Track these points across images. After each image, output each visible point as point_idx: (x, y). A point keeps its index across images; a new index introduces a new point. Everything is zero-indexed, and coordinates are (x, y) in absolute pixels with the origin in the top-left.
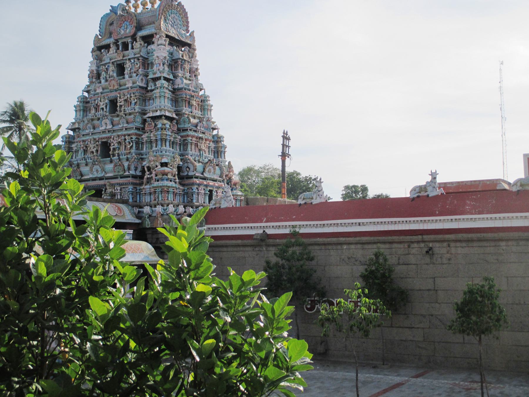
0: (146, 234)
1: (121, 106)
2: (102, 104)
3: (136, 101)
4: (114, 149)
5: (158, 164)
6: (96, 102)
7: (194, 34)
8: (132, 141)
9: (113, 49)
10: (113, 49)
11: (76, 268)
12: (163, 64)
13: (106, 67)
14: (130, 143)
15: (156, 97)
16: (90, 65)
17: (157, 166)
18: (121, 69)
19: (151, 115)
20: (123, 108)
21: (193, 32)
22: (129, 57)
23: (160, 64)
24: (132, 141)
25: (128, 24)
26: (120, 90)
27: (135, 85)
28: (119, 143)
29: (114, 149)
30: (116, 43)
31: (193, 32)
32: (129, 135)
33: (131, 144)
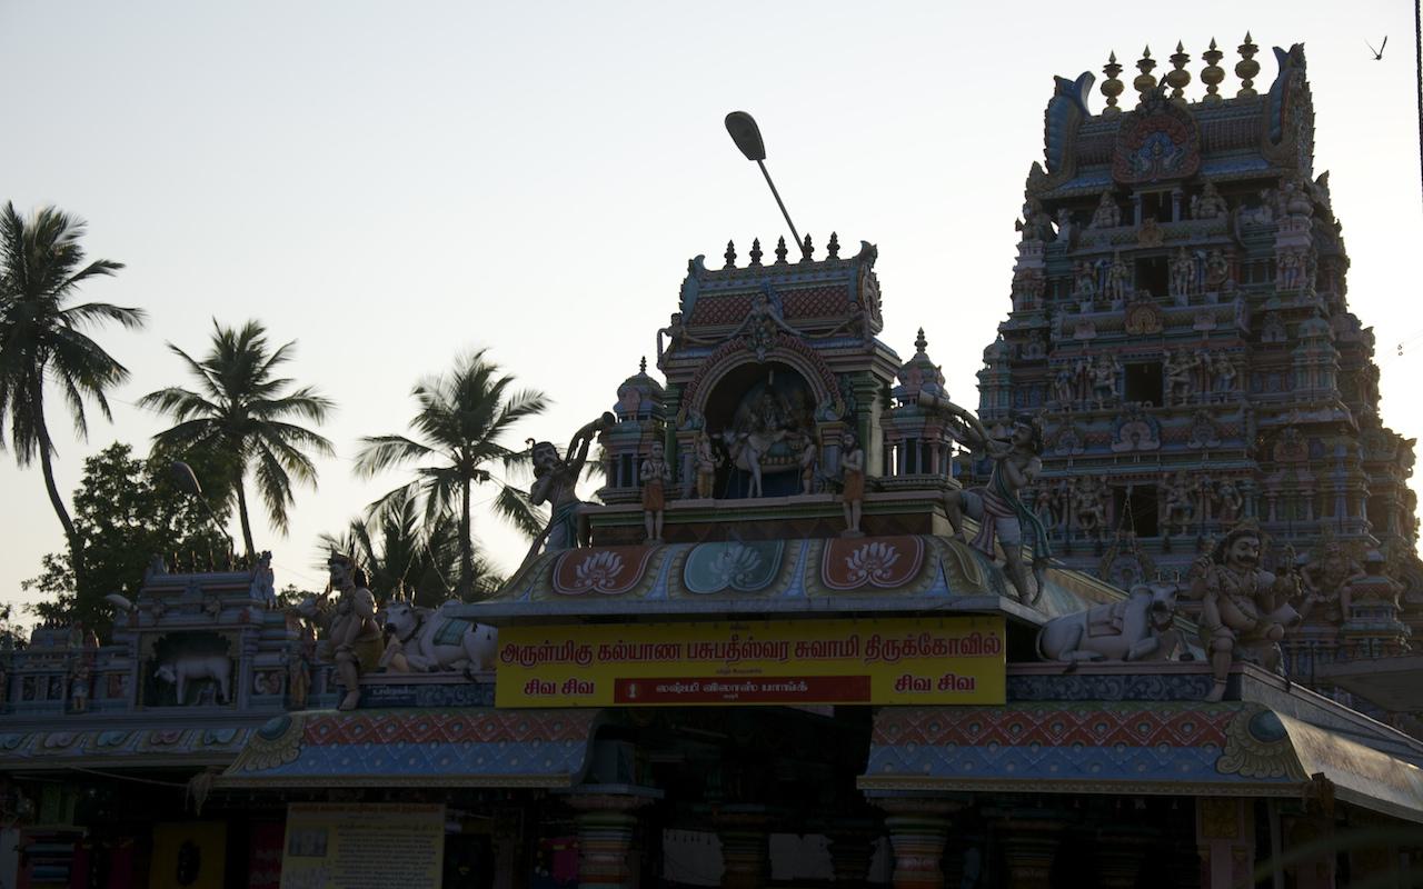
0: (745, 546)
1: (1179, 386)
2: (1101, 374)
3: (1234, 373)
4: (1178, 512)
5: (1356, 565)
6: (1079, 368)
7: (1329, 179)
8: (1241, 492)
9: (1105, 214)
10: (1105, 214)
11: (715, 690)
12: (1308, 272)
13: (1098, 264)
14: (1234, 498)
15: (1305, 367)
16: (1018, 254)
17: (1353, 572)
18: (1153, 275)
19: (1298, 418)
20: (1185, 393)
21: (1326, 174)
22: (1191, 242)
23: (1298, 270)
24: (1241, 492)
25: (1166, 140)
26: (1167, 338)
27: (1226, 327)
28: (1193, 496)
29: (1178, 512)
30: (1122, 195)
31: (1326, 174)
32: (1232, 473)
33: (1240, 501)
